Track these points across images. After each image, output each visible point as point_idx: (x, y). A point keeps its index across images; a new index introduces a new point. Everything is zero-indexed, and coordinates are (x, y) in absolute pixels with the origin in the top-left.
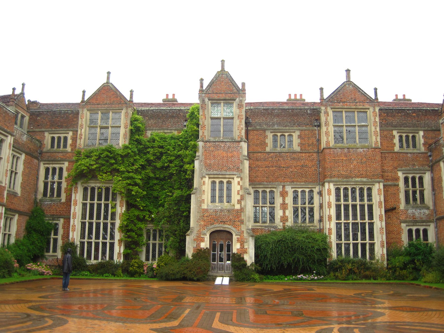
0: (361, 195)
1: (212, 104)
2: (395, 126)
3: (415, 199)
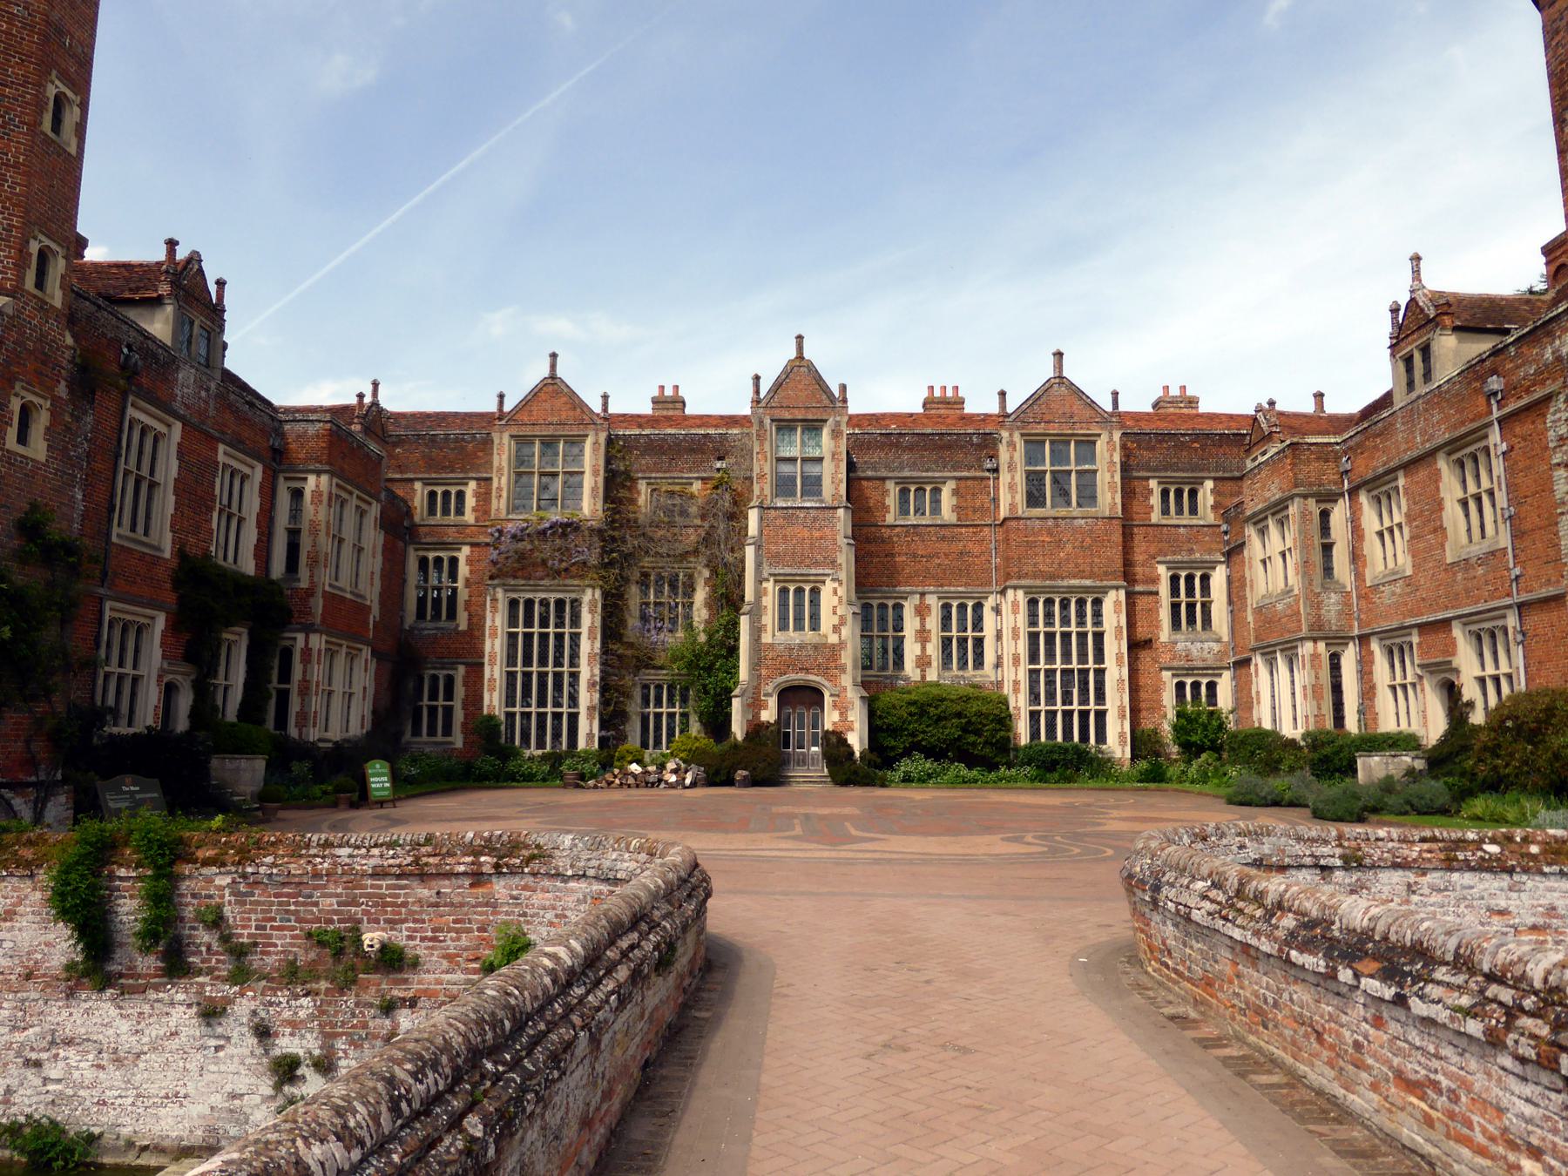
1: (779, 429)
3: (1191, 620)
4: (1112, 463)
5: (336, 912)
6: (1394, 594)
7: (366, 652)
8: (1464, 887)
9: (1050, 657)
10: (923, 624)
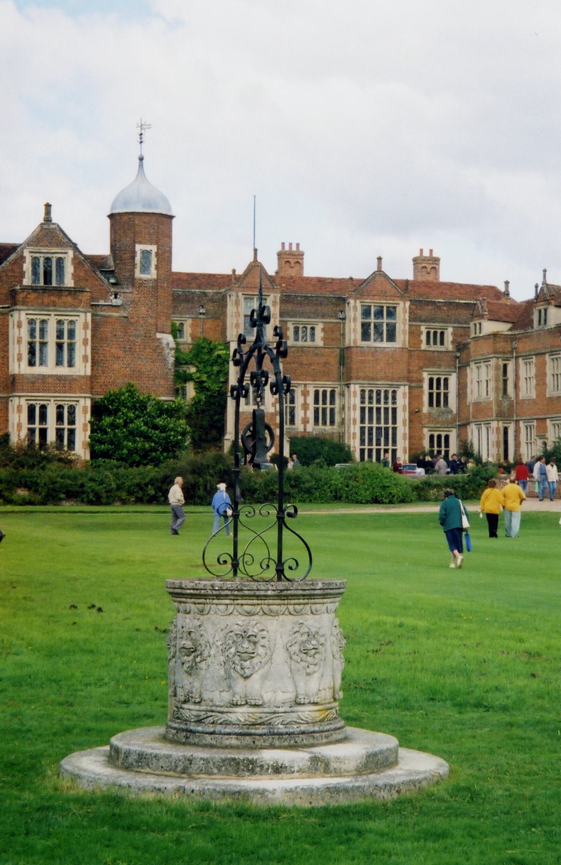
0: (386, 398)
1: (245, 299)
2: (424, 321)
4: (405, 319)
10: (305, 400)
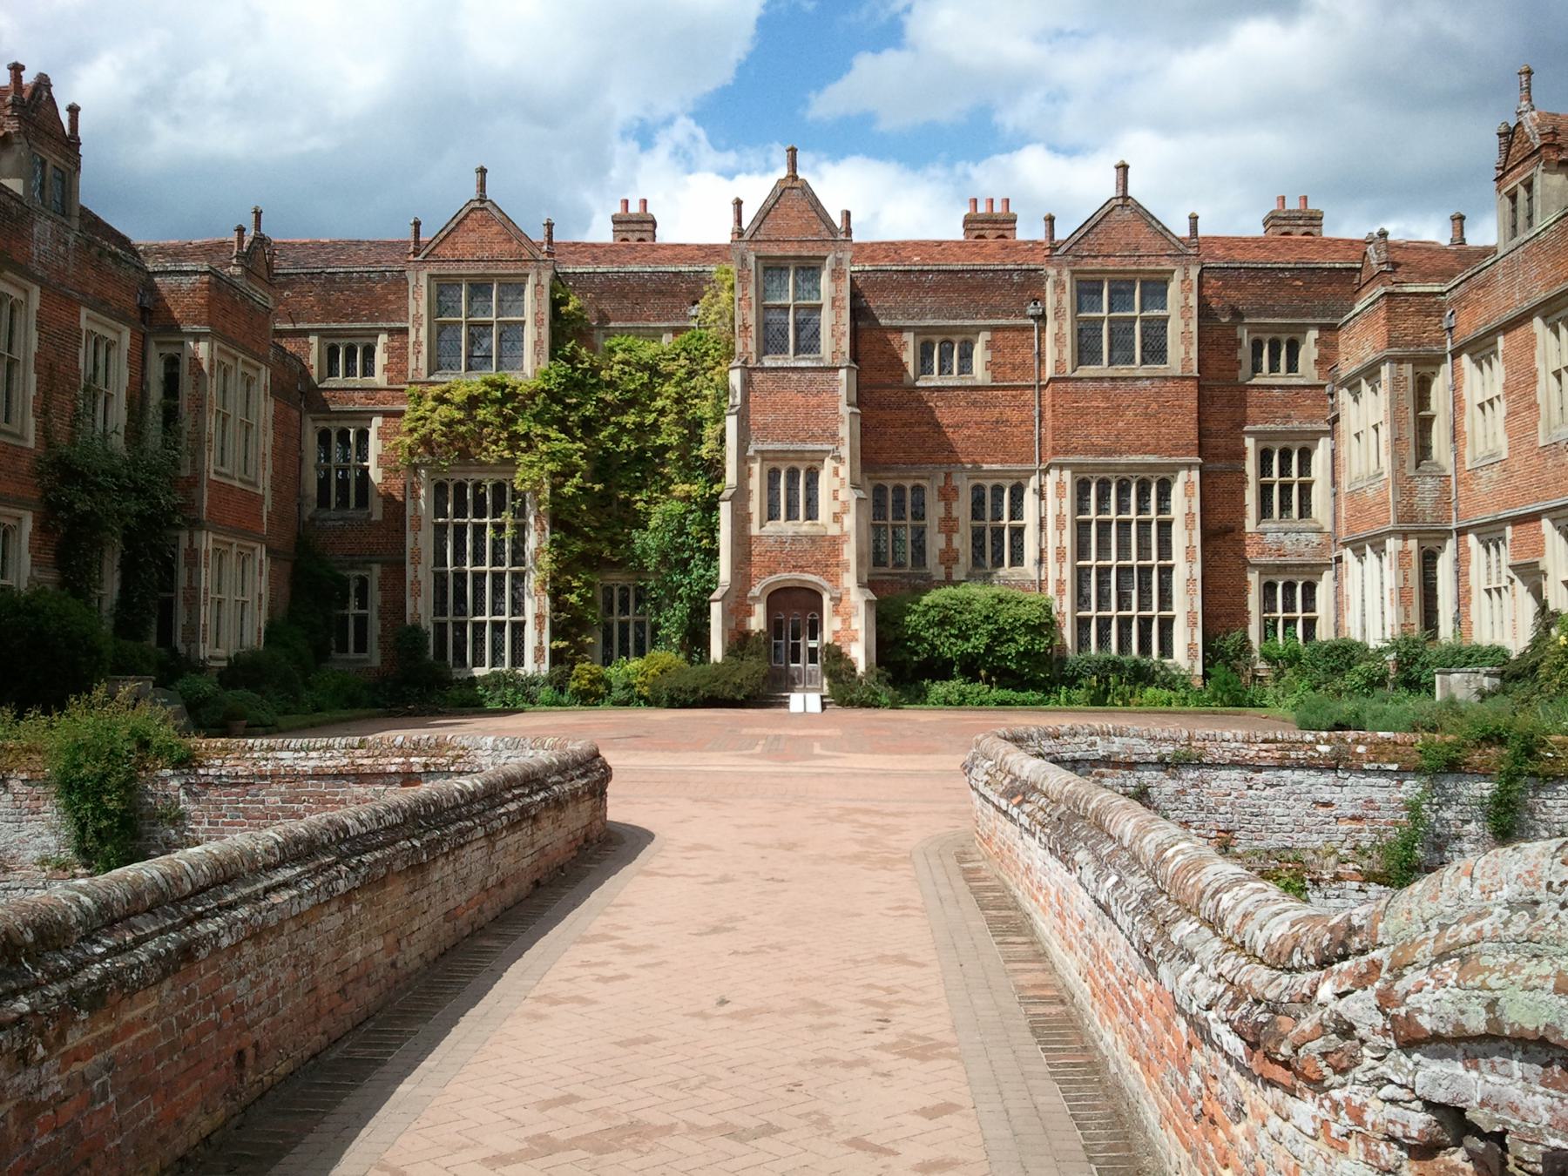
3: (1285, 507)
5: (280, 809)
6: (1490, 480)
7: (261, 552)
8: (1294, 783)
9: (1103, 551)
